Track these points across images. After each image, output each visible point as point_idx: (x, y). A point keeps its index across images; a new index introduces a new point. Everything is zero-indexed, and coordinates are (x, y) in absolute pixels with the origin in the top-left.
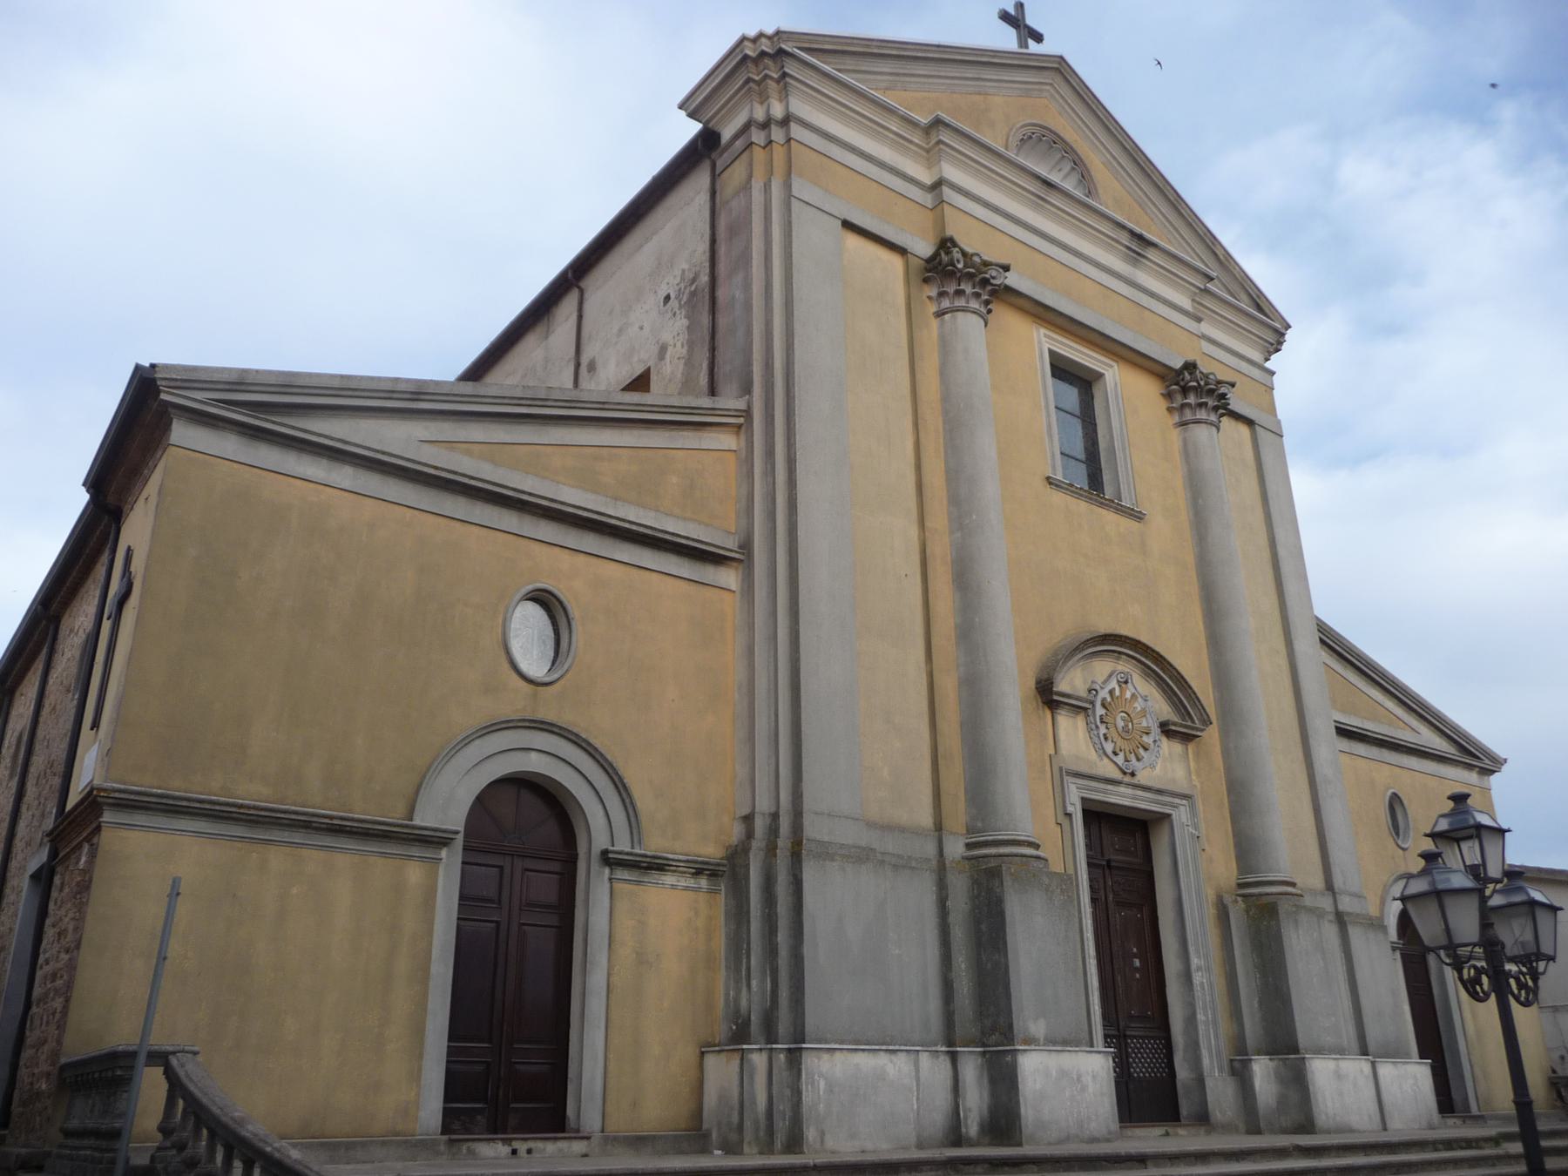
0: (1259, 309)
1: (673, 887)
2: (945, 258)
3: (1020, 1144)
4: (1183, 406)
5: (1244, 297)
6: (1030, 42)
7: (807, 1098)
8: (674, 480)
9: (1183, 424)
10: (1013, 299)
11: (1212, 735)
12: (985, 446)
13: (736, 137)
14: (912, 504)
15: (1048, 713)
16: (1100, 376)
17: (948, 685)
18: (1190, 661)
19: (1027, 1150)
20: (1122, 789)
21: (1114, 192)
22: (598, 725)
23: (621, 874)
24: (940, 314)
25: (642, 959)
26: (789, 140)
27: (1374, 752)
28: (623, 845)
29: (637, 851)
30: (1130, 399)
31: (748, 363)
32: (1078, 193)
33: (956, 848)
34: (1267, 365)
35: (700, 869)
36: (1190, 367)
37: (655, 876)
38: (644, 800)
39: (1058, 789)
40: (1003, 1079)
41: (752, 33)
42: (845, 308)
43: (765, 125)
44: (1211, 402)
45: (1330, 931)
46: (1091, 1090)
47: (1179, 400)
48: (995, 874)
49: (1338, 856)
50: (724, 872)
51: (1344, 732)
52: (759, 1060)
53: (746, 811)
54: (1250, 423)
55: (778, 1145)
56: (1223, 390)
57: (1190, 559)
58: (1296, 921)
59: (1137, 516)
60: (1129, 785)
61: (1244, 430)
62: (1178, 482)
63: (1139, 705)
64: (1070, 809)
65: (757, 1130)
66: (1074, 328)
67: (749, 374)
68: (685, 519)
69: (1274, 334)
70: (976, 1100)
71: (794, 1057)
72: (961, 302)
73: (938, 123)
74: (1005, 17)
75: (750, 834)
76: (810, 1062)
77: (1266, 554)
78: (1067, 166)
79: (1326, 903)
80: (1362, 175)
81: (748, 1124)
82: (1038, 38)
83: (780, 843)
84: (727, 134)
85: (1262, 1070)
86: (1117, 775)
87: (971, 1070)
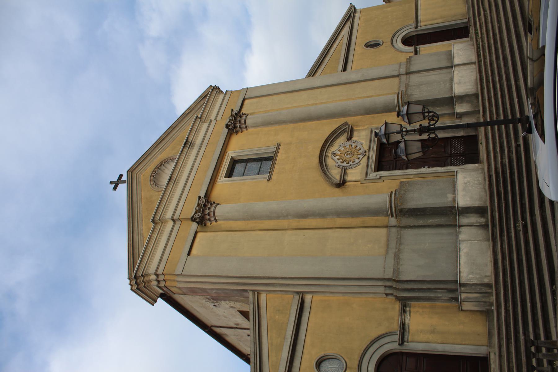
0: (206, 96)
1: (409, 320)
2: (198, 220)
3: (487, 207)
4: (240, 128)
5: (202, 102)
6: (123, 179)
7: (475, 282)
8: (277, 317)
9: (246, 128)
10: (209, 192)
11: (350, 120)
12: (260, 206)
13: (162, 290)
14: (280, 232)
15: (347, 184)
16: (232, 157)
17: (340, 221)
18: (327, 128)
19: (488, 204)
20: (370, 156)
21: (171, 149)
22: (358, 346)
23: (406, 338)
24: (216, 221)
25: (433, 332)
26: (163, 274)
27: (351, 53)
28: (397, 338)
29: (398, 333)
30: (239, 146)
31: (237, 290)
32: (173, 165)
33: (393, 221)
34: (224, 92)
35: (403, 311)
36: (227, 126)
37: (406, 326)
38: (382, 330)
39: (372, 181)
40: (466, 211)
41: (130, 287)
42: (217, 254)
43: (159, 281)
44: (239, 119)
45: (414, 79)
46: (469, 179)
47: (238, 129)
48: (401, 211)
49: (387, 73)
50: (404, 303)
51: (345, 69)
52: (463, 296)
53: (384, 295)
54: (244, 100)
55: (490, 291)
56: (234, 114)
57: (292, 125)
58: (411, 95)
59: (278, 146)
60: (369, 154)
61: (246, 102)
62: (266, 129)
63: (342, 149)
64: (378, 177)
65: (485, 297)
66: (217, 169)
67: (241, 290)
68: (290, 314)
69: (215, 90)
70: (473, 219)
71: (462, 285)
72: (212, 214)
73: (153, 221)
74: (115, 188)
75: (392, 294)
76: (463, 281)
77: (288, 95)
78: (163, 167)
79: (404, 78)
80: (155, 28)
81: (484, 300)
82: (121, 176)
83: (394, 286)
84: (161, 291)
85: (460, 108)
86: (366, 158)
87: (464, 220)
